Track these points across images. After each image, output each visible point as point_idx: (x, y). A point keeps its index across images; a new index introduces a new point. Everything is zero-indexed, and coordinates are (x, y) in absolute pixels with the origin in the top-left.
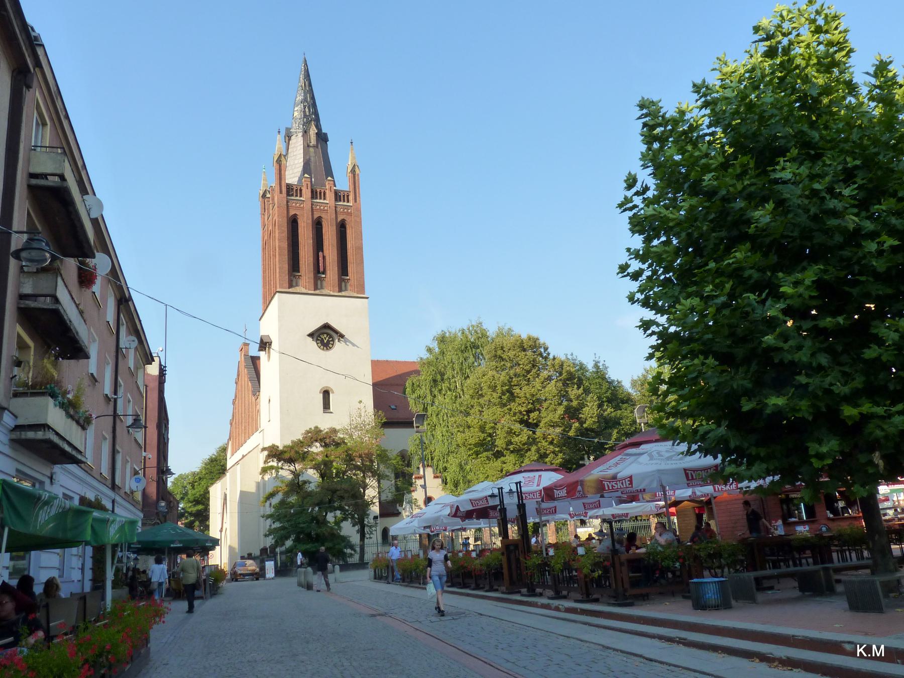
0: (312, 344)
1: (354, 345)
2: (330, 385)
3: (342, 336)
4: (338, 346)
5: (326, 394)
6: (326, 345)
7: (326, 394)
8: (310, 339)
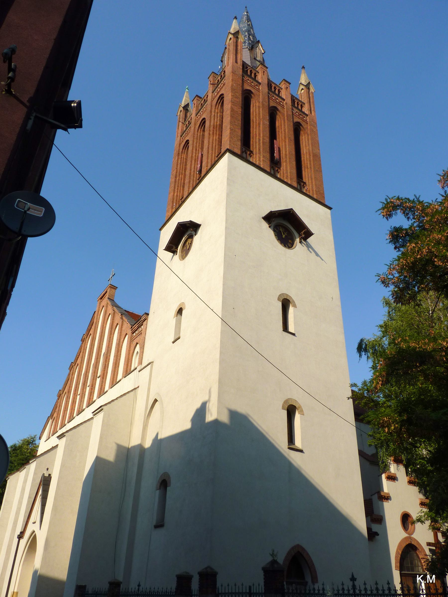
0: (268, 233)
1: (317, 255)
2: (293, 295)
3: (308, 234)
4: (299, 247)
5: (286, 304)
6: (286, 241)
7: (286, 304)
8: (265, 225)
